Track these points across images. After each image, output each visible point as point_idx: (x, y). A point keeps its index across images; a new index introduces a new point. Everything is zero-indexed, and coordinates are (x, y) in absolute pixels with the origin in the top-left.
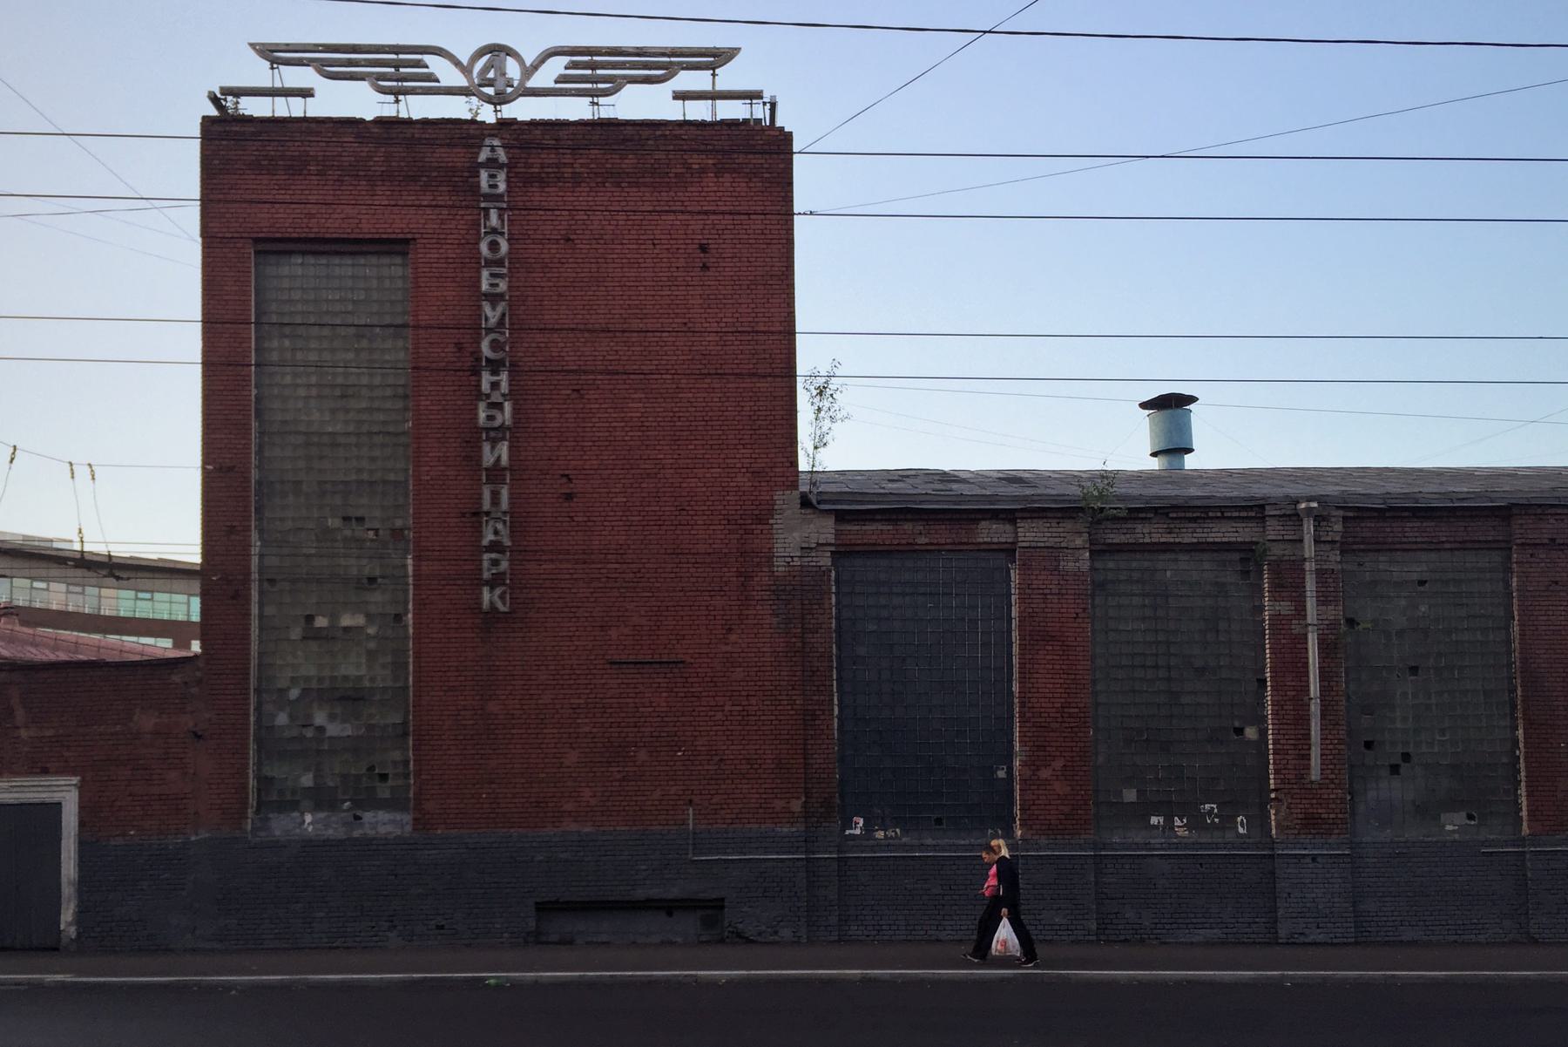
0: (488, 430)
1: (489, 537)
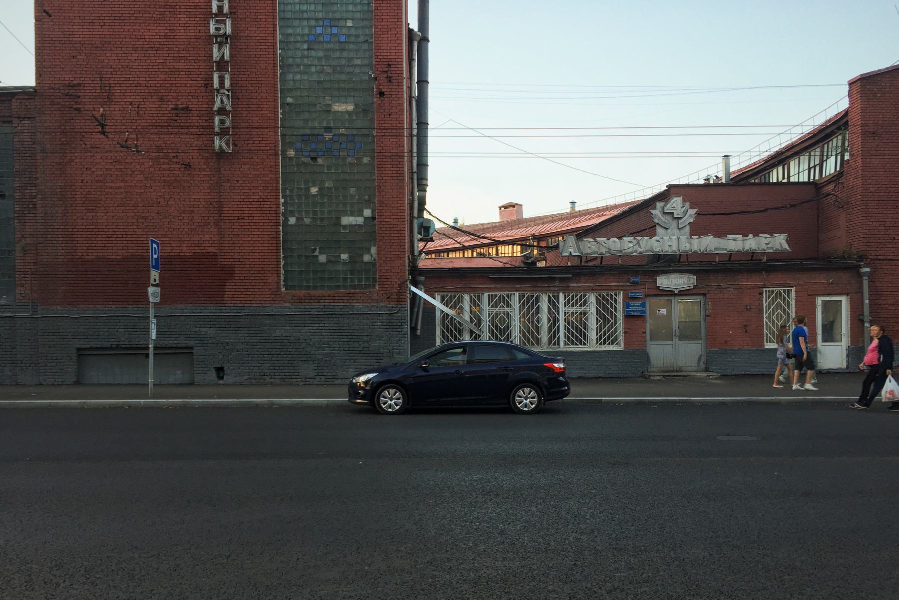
0: (216, 37)
1: (217, 105)
